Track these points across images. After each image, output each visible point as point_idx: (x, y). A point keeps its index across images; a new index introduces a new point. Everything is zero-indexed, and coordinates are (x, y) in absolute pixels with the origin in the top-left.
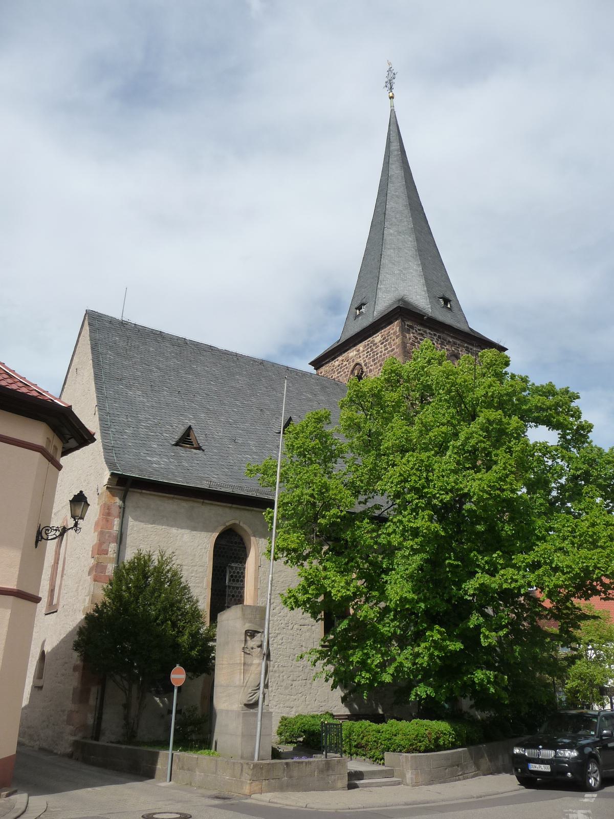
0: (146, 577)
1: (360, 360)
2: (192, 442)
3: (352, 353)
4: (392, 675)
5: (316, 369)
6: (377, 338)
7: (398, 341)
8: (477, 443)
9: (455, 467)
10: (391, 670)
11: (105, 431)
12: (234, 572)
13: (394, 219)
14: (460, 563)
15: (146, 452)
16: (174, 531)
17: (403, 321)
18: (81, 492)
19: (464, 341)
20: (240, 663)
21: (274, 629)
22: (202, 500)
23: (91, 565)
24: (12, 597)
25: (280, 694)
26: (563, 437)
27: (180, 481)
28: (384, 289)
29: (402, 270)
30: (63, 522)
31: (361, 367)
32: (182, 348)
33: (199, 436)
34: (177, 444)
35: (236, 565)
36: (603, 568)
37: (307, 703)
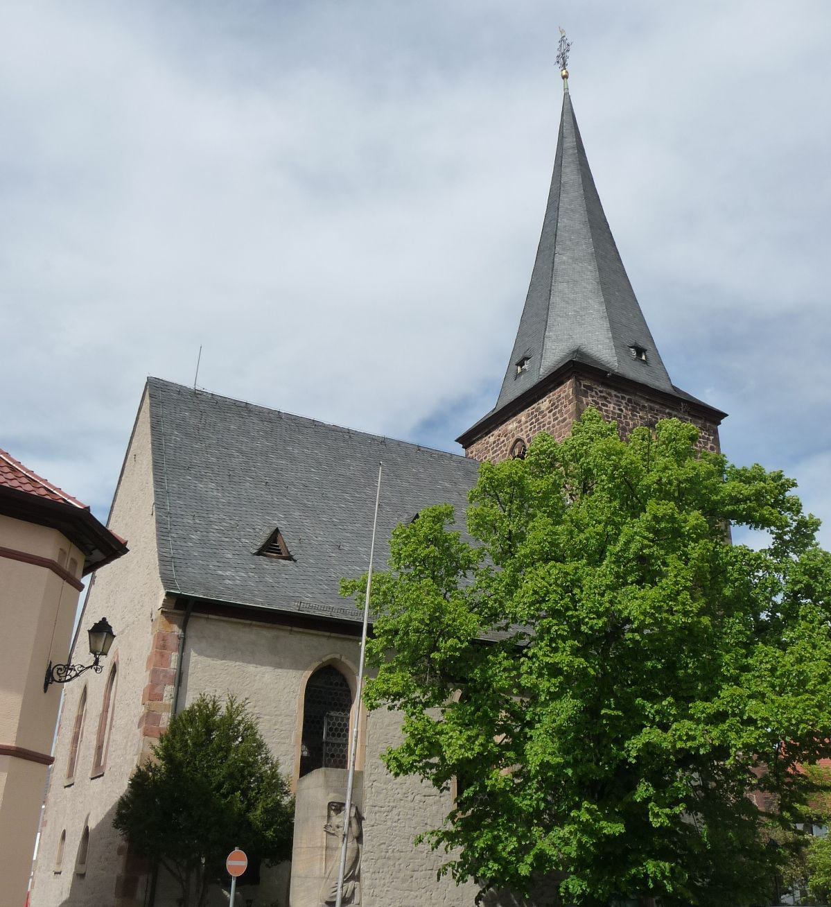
0: (209, 732)
1: (523, 435)
2: (280, 550)
3: (511, 425)
4: (531, 865)
5: (466, 447)
6: (544, 404)
7: (571, 407)
8: (641, 550)
9: (611, 582)
10: (529, 859)
11: (162, 537)
12: (334, 724)
13: (568, 242)
14: (621, 714)
15: (218, 564)
16: (251, 668)
17: (577, 380)
18: (104, 619)
19: (666, 406)
20: (321, 847)
21: (388, 800)
22: (290, 628)
23: (142, 714)
24: (9, 757)
25: (395, 889)
26: (779, 537)
27: (259, 602)
28: (554, 337)
29: (578, 310)
30: (114, 657)
31: (523, 444)
32: (273, 424)
33: (289, 541)
34: (259, 553)
35: (337, 714)
36: (810, 720)
37: (433, 901)
